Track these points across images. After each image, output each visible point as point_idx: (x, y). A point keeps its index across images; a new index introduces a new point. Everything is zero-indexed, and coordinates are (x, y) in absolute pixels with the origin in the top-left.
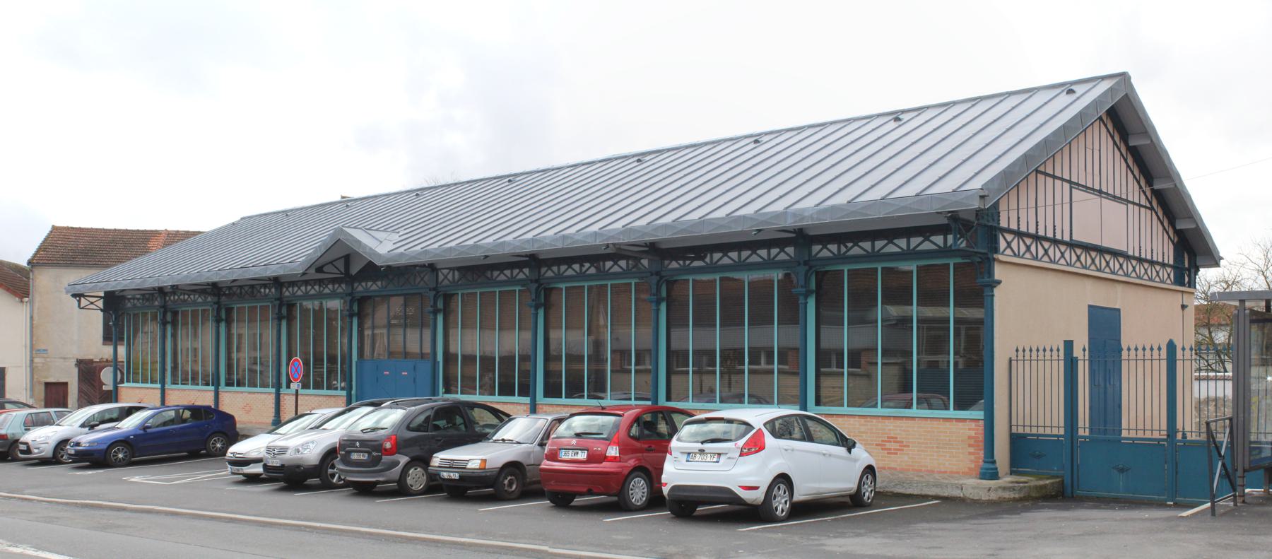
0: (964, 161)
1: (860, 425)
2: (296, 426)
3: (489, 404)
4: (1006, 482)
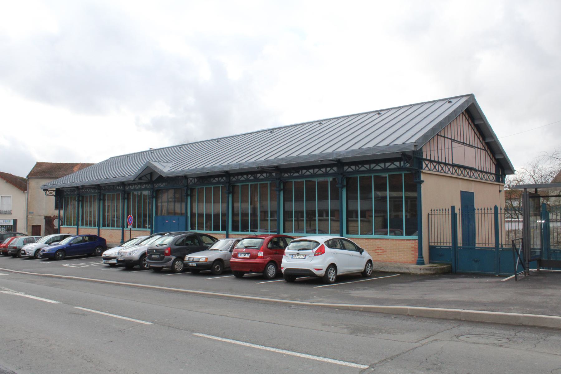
0: (408, 131)
1: (366, 242)
2: (130, 243)
3: (209, 234)
4: (427, 266)
